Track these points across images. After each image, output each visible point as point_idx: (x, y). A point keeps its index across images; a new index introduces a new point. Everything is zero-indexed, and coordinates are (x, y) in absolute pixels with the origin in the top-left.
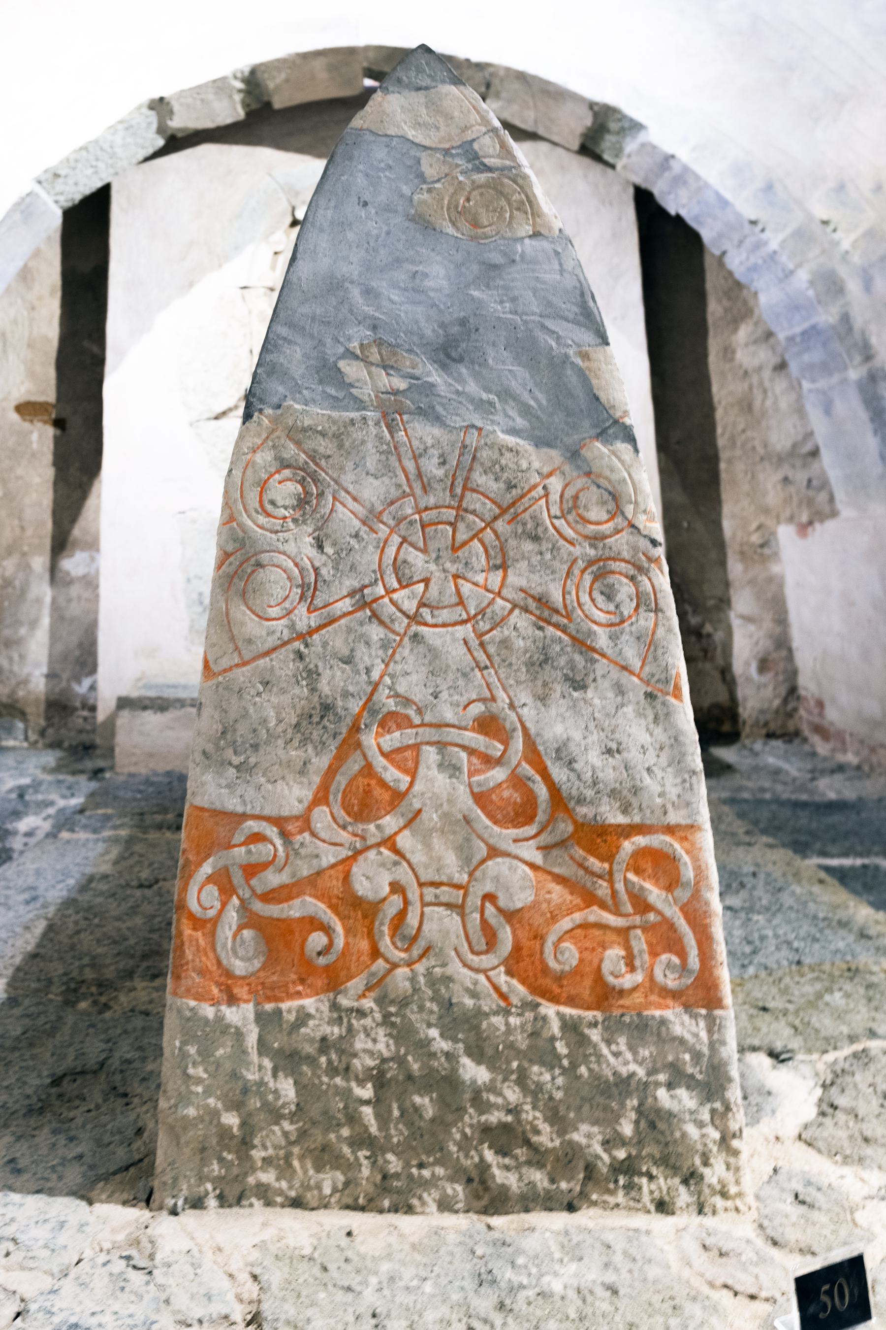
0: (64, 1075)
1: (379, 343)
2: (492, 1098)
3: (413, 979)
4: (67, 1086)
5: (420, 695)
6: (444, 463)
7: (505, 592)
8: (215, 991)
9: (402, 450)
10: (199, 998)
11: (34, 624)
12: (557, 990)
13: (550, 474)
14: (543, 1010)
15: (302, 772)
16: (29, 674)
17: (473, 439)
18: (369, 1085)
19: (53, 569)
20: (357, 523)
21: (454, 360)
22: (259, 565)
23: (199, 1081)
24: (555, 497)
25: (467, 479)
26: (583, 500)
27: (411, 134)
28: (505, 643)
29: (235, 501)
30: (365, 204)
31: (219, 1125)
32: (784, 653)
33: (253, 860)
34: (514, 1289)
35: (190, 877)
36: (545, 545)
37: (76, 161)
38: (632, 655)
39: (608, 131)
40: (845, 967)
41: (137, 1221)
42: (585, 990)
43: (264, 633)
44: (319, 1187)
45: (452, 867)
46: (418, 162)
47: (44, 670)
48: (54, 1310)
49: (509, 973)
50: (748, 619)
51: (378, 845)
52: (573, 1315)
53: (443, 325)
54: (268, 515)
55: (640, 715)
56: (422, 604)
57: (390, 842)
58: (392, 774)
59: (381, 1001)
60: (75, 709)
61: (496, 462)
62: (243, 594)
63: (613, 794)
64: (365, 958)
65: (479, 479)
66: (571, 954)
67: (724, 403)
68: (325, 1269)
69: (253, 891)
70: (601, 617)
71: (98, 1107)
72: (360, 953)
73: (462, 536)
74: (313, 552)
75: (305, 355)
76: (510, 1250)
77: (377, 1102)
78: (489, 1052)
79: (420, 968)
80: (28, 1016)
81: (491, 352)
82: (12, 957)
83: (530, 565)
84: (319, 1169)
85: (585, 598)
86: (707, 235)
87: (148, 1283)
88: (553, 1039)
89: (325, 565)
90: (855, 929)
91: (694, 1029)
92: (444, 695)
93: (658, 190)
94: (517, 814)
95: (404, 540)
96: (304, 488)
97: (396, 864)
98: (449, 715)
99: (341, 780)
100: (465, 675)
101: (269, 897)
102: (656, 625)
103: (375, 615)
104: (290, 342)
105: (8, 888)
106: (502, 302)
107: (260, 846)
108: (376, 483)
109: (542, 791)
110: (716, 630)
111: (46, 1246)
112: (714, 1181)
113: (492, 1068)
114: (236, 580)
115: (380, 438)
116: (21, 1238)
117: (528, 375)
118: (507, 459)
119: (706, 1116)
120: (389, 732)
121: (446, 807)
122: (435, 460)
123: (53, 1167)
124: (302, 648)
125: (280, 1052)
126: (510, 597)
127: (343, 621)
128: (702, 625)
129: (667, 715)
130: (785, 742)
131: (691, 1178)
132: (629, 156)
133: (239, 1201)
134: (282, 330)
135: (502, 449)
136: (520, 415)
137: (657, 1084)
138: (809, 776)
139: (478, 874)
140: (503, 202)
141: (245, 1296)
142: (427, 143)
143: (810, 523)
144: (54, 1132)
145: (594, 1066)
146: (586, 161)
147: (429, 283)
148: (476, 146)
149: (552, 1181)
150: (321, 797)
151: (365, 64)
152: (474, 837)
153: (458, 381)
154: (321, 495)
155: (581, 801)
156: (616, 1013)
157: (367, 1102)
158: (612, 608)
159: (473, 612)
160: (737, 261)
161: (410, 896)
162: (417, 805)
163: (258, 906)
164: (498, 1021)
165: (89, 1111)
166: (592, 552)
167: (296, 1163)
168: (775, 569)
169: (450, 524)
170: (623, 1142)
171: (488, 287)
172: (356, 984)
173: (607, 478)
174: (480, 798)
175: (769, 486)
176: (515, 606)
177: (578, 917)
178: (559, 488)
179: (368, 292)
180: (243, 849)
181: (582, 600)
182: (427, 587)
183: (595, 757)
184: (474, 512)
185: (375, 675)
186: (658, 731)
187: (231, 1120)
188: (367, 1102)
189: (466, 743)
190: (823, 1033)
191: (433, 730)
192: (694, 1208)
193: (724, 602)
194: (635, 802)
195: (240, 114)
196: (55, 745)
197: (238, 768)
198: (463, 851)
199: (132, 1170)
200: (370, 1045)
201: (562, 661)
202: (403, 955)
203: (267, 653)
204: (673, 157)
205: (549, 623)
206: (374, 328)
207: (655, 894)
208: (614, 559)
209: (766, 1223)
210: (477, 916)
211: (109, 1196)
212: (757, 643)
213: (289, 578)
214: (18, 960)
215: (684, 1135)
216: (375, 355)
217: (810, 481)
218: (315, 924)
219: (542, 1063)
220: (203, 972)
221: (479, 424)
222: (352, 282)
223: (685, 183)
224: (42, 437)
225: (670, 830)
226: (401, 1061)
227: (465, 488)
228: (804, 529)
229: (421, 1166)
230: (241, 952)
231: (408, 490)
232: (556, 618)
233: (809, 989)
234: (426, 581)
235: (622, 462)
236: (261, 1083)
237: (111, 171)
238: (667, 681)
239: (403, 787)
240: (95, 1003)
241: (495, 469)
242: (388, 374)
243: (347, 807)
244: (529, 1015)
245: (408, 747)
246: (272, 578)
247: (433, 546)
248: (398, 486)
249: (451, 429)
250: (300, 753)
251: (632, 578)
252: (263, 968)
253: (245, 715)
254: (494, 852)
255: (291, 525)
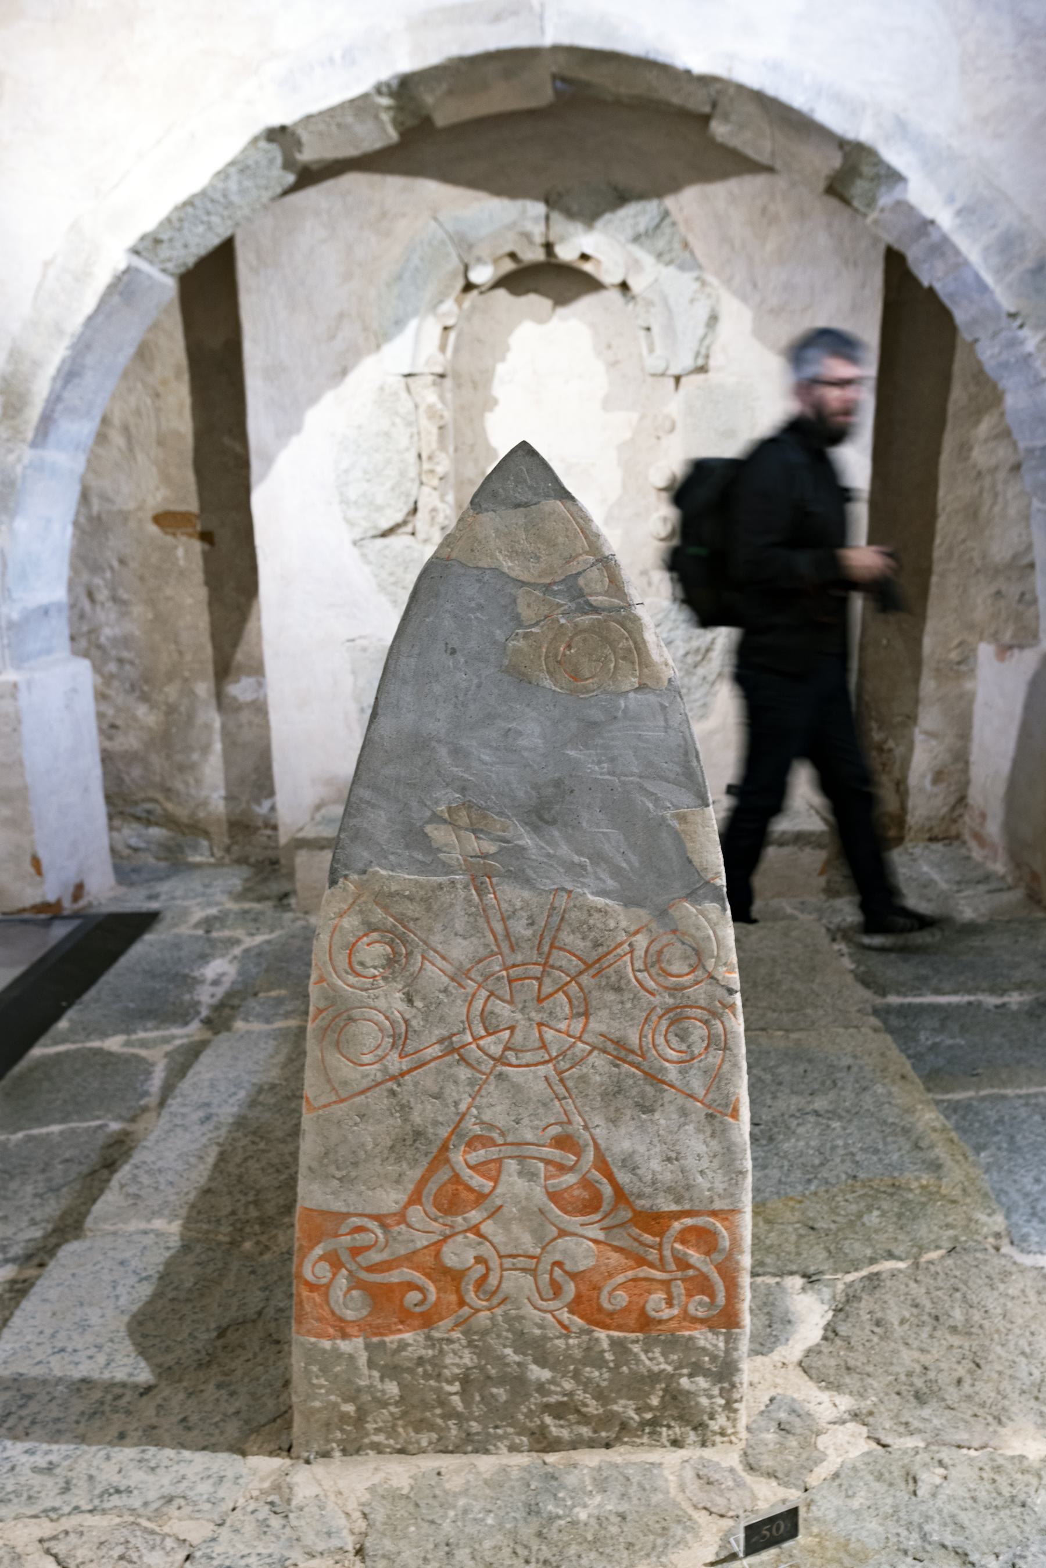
0: (229, 1326)
1: (469, 806)
2: (553, 1388)
3: (492, 1319)
4: (232, 1337)
5: (501, 1122)
6: (532, 924)
7: (585, 1037)
8: (331, 1331)
9: (491, 912)
10: (319, 1336)
11: (206, 749)
12: (608, 1321)
13: (637, 932)
14: (596, 1335)
15: (398, 1182)
16: (207, 797)
17: (562, 901)
18: (457, 1383)
19: (219, 695)
20: (445, 980)
21: (547, 822)
22: (351, 1019)
23: (321, 1387)
24: (640, 952)
25: (555, 938)
26: (667, 954)
27: (507, 565)
28: (583, 1079)
29: (325, 963)
30: (453, 652)
31: (339, 1411)
32: (960, 766)
33: (357, 1244)
34: (552, 1518)
35: (304, 1257)
36: (627, 995)
37: (181, 220)
38: (697, 1086)
39: (860, 175)
40: (890, 1183)
41: (279, 1469)
42: (632, 1320)
43: (359, 1076)
44: (418, 1442)
45: (528, 1242)
46: (514, 601)
47: (222, 792)
48: (214, 1555)
49: (571, 1312)
50: (931, 735)
51: (465, 1231)
52: (590, 1538)
53: (536, 787)
54: (358, 975)
55: (699, 1131)
56: (507, 1048)
57: (475, 1230)
58: (477, 1181)
59: (465, 1333)
60: (258, 828)
61: (585, 922)
62: (337, 1044)
63: (669, 1190)
64: (454, 1307)
65: (567, 938)
66: (622, 1298)
67: (948, 510)
68: (417, 1505)
69: (359, 1265)
70: (672, 1055)
71: (255, 1355)
72: (449, 1303)
73: (547, 989)
74: (403, 1006)
75: (389, 820)
76: (555, 1483)
77: (463, 1393)
78: (551, 1360)
79: (498, 1311)
80: (199, 1264)
81: (585, 815)
82: (187, 1193)
83: (611, 1013)
84: (417, 1432)
85: (660, 1040)
86: (960, 316)
87: (284, 1526)
88: (603, 1351)
89: (414, 1017)
90: (913, 1138)
91: (715, 1342)
92: (526, 1121)
93: (913, 254)
94: (585, 1207)
95: (492, 994)
96: (392, 949)
97: (479, 1244)
98: (529, 1136)
99: (432, 1187)
100: (545, 1105)
101: (371, 1269)
102: (723, 1061)
103: (462, 1058)
104: (373, 806)
105: (184, 1105)
106: (599, 762)
107: (363, 1235)
108: (465, 943)
109: (607, 1190)
110: (897, 745)
111: (208, 1501)
112: (716, 1428)
113: (553, 1369)
114: (329, 1032)
115: (468, 901)
116: (190, 1494)
117: (622, 837)
118: (595, 919)
119: (716, 1391)
120: (475, 1150)
121: (524, 1203)
122: (524, 921)
123: (216, 1424)
124: (395, 1087)
125: (385, 1366)
126: (590, 1040)
127: (432, 1064)
128: (885, 741)
129: (724, 1131)
130: (945, 845)
131: (699, 1427)
132: (882, 210)
133: (357, 1452)
134: (366, 794)
135: (591, 910)
136: (612, 878)
137: (681, 1375)
138: (955, 888)
139: (549, 1248)
140: (608, 651)
141: (356, 1530)
142: (525, 577)
143: (1010, 647)
144: (219, 1386)
145: (633, 1367)
146: (833, 203)
147: (523, 742)
148: (581, 581)
149: (595, 1432)
150: (415, 1198)
151: (554, 69)
152: (547, 1223)
153: (548, 843)
154: (409, 954)
155: (640, 1196)
156: (654, 1334)
157: (455, 1394)
158: (684, 1047)
159: (554, 1054)
160: (988, 353)
161: (491, 1265)
162: (498, 1202)
163: (364, 1275)
164: (560, 1343)
165: (248, 1360)
166: (671, 1001)
167: (401, 1430)
168: (968, 685)
169: (537, 979)
170: (650, 1409)
171: (586, 746)
172: (447, 1323)
173: (692, 936)
174: (554, 1196)
175: (979, 601)
176: (594, 1048)
177: (630, 1274)
178: (645, 945)
179: (456, 752)
180: (349, 1237)
181: (657, 1042)
182: (512, 1033)
183: (655, 1165)
184: (560, 968)
185: (463, 1107)
186: (714, 1144)
187: (349, 1408)
188: (455, 1394)
189: (544, 1156)
190: (851, 1256)
191: (514, 1148)
192: (698, 1445)
193: (911, 718)
194: (687, 1195)
195: (393, 135)
196: (242, 861)
197: (340, 1180)
198: (538, 1235)
199: (279, 1421)
200: (457, 1360)
201: (634, 1092)
202: (485, 1303)
203: (363, 1092)
204: (932, 222)
205: (625, 1061)
206: (463, 790)
207: (695, 1256)
208: (691, 1007)
209: (750, 1451)
210: (547, 1276)
211: (260, 1448)
212: (935, 757)
213: (381, 1030)
214: (192, 1196)
215: (697, 1404)
216: (464, 819)
217: (1023, 594)
218: (411, 1286)
219: (593, 1365)
220: (320, 1319)
221: (569, 887)
222: (439, 741)
223: (943, 254)
224: (188, 552)
225: (714, 1213)
226: (482, 1369)
227: (552, 946)
228: (1004, 650)
229: (496, 1427)
230: (351, 1305)
231: (496, 949)
232: (631, 1057)
233: (853, 1208)
234: (512, 1029)
235: (708, 920)
236: (371, 1386)
237: (230, 223)
238: (727, 1105)
239: (487, 1190)
240: (258, 1243)
241: (583, 929)
242: (477, 838)
243: (438, 1206)
244: (585, 1338)
245: (493, 1160)
246: (365, 1030)
247: (519, 998)
248: (487, 946)
249: (541, 893)
250: (396, 1168)
251: (706, 1022)
252: (370, 1314)
253: (345, 1140)
254: (563, 1233)
255: (381, 983)
